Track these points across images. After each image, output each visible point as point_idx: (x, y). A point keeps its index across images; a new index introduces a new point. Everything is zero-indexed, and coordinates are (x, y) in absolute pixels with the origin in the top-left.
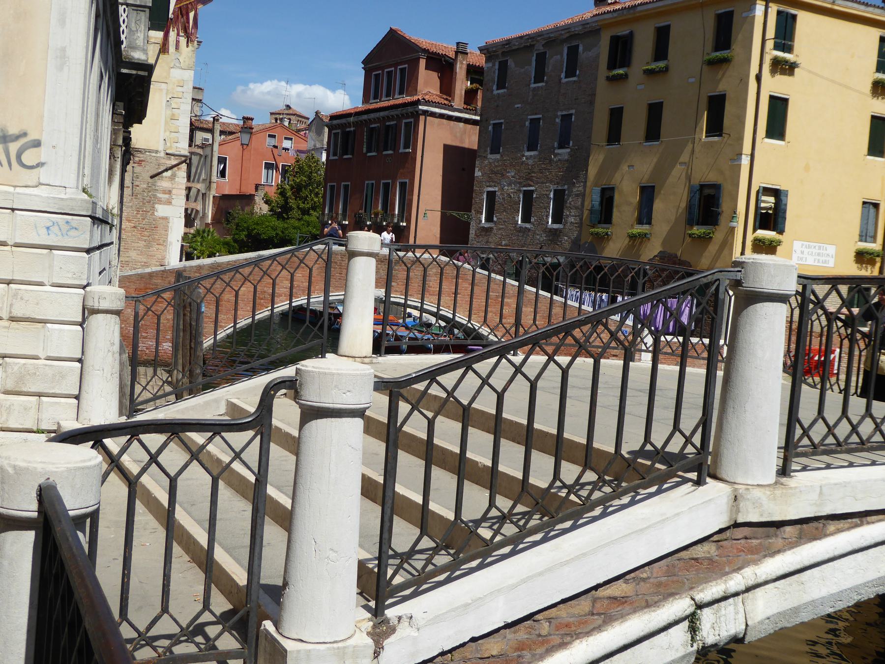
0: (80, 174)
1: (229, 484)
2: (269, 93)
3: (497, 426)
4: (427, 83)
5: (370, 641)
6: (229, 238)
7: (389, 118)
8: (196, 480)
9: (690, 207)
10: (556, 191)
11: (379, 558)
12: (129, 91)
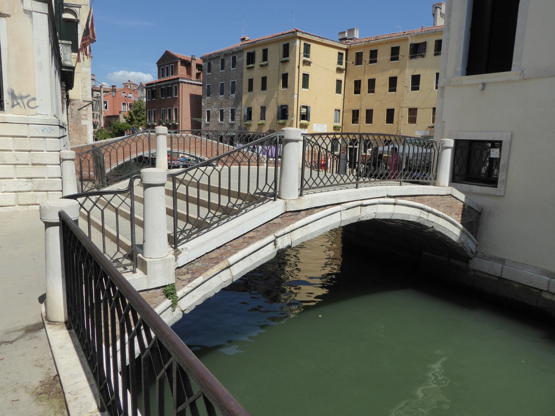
0: (53, 110)
1: (122, 216)
2: (122, 76)
3: (209, 189)
4: (181, 70)
5: (174, 256)
6: (111, 132)
7: (168, 85)
8: (110, 214)
9: (278, 113)
10: (231, 110)
11: (174, 233)
12: (67, 78)
